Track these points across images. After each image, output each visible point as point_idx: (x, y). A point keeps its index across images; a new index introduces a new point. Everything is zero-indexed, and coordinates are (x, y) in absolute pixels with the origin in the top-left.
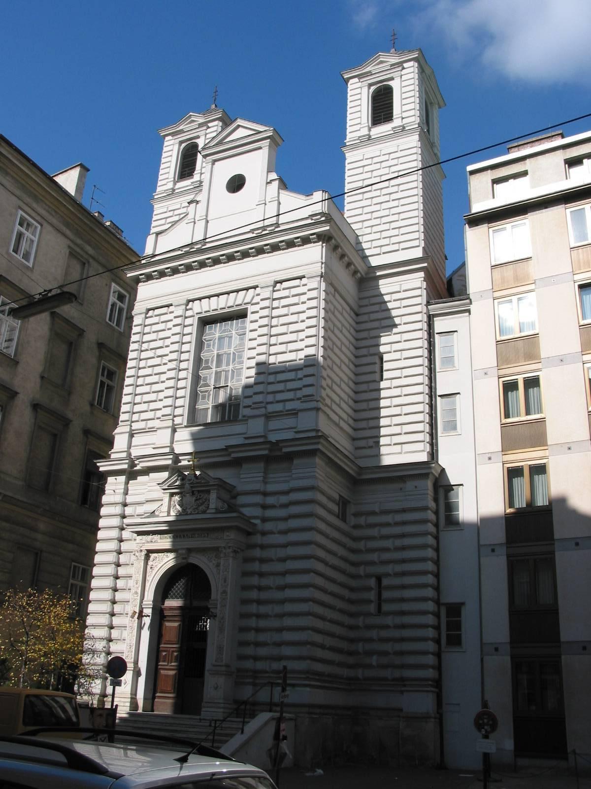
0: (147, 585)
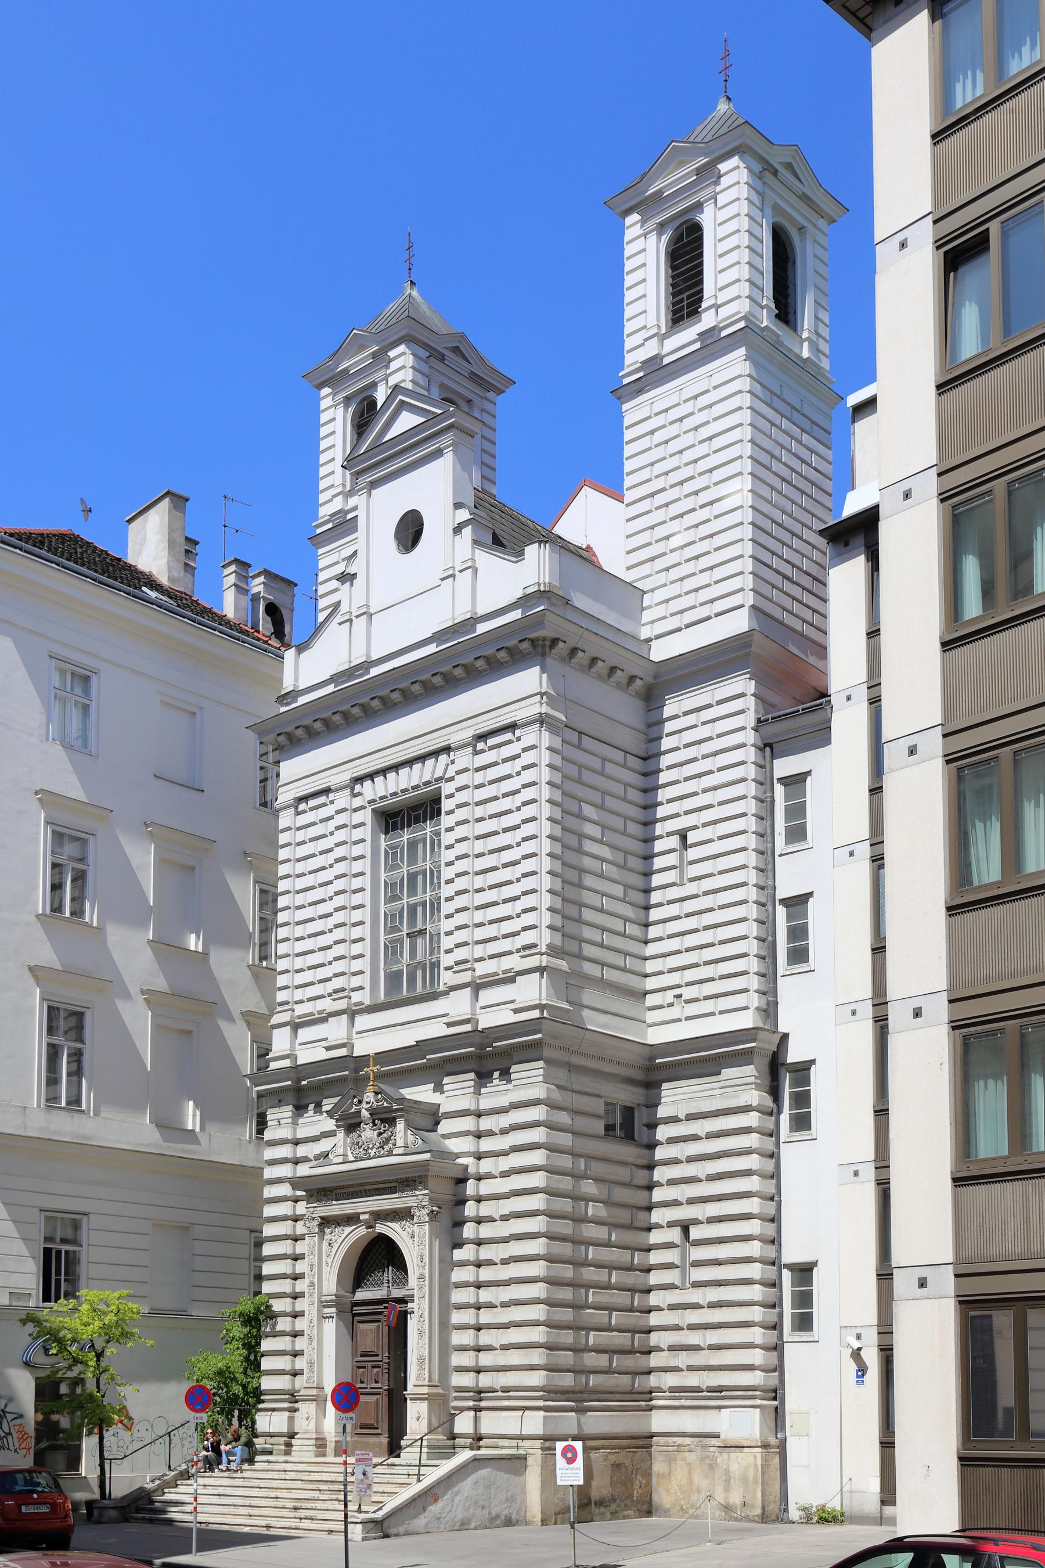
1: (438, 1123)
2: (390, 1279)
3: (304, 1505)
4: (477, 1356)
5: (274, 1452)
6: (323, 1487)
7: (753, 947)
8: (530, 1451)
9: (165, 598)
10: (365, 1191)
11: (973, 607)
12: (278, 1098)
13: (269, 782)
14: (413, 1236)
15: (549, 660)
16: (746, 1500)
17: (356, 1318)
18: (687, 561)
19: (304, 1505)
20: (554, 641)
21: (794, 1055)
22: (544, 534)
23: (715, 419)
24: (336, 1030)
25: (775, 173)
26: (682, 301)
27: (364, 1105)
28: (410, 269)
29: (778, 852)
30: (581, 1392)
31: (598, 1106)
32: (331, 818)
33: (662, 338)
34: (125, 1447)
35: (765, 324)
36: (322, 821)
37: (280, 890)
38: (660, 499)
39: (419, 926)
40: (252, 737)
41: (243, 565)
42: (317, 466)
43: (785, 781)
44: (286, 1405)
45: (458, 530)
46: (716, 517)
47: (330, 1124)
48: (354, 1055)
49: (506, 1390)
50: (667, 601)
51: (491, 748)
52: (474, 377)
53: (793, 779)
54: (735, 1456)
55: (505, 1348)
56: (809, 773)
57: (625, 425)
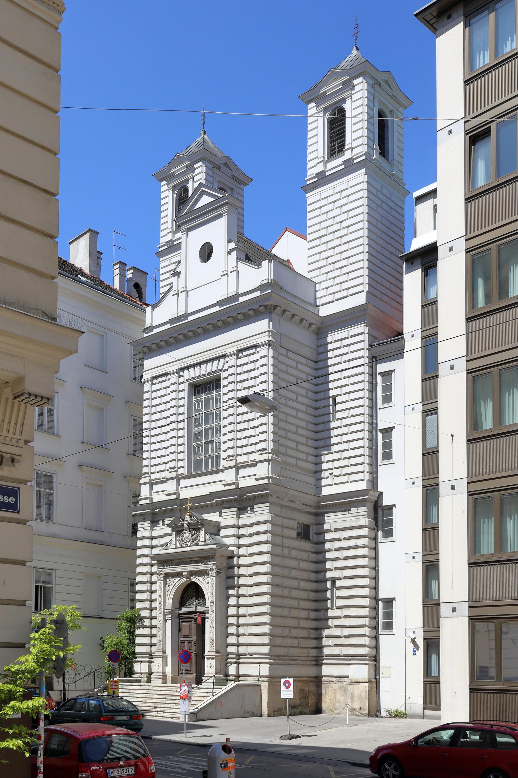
0: (167, 597)
1: (219, 531)
2: (197, 602)
3: (159, 705)
4: (238, 639)
5: (142, 681)
6: (167, 697)
7: (367, 451)
8: (262, 683)
9: (89, 281)
10: (186, 562)
11: (481, 303)
12: (144, 518)
13: (137, 368)
14: (208, 583)
15: (273, 316)
16: (361, 706)
17: (181, 620)
18: (337, 269)
19: (159, 705)
20: (275, 307)
21: (386, 502)
22: (268, 254)
23: (351, 202)
24: (171, 486)
25: (380, 85)
26: (335, 145)
27: (185, 522)
28: (203, 125)
29: (378, 407)
30: (286, 656)
31: (294, 524)
32: (169, 387)
33: (326, 163)
34: (72, 678)
35: (375, 157)
36: (164, 388)
37: (144, 420)
38: (324, 240)
39: (210, 439)
40: (130, 348)
41: (123, 264)
42: (159, 218)
43: (382, 374)
44: (147, 660)
45: (229, 252)
46: (351, 249)
47: (169, 530)
48: (180, 498)
49: (251, 654)
50: (327, 288)
51: (245, 356)
52: (234, 178)
53: (385, 373)
54: (356, 686)
55: (251, 635)
56: (393, 371)
57: (307, 204)
